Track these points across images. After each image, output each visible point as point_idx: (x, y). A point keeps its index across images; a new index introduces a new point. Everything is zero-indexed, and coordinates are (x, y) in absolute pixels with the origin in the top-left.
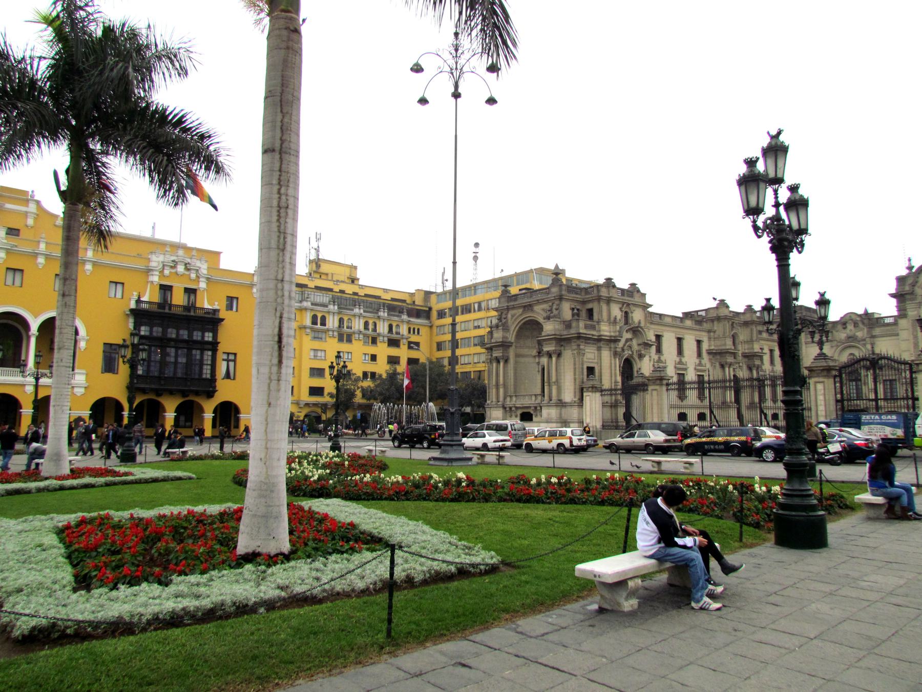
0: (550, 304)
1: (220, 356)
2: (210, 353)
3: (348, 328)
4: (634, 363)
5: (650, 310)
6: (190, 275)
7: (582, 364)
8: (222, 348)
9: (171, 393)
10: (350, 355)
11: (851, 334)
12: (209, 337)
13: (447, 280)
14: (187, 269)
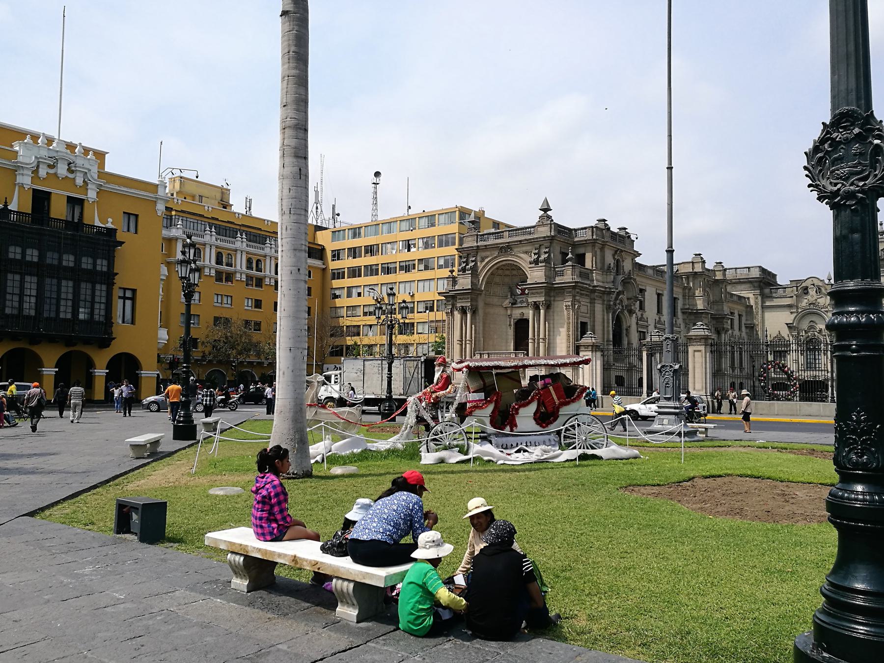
0: (537, 246)
1: (117, 293)
2: (104, 287)
3: (227, 265)
4: (624, 320)
5: (638, 260)
6: (74, 179)
7: (577, 319)
8: (120, 281)
9: (52, 340)
10: (229, 299)
11: (812, 300)
12: (102, 265)
13: (338, 215)
14: (70, 170)
